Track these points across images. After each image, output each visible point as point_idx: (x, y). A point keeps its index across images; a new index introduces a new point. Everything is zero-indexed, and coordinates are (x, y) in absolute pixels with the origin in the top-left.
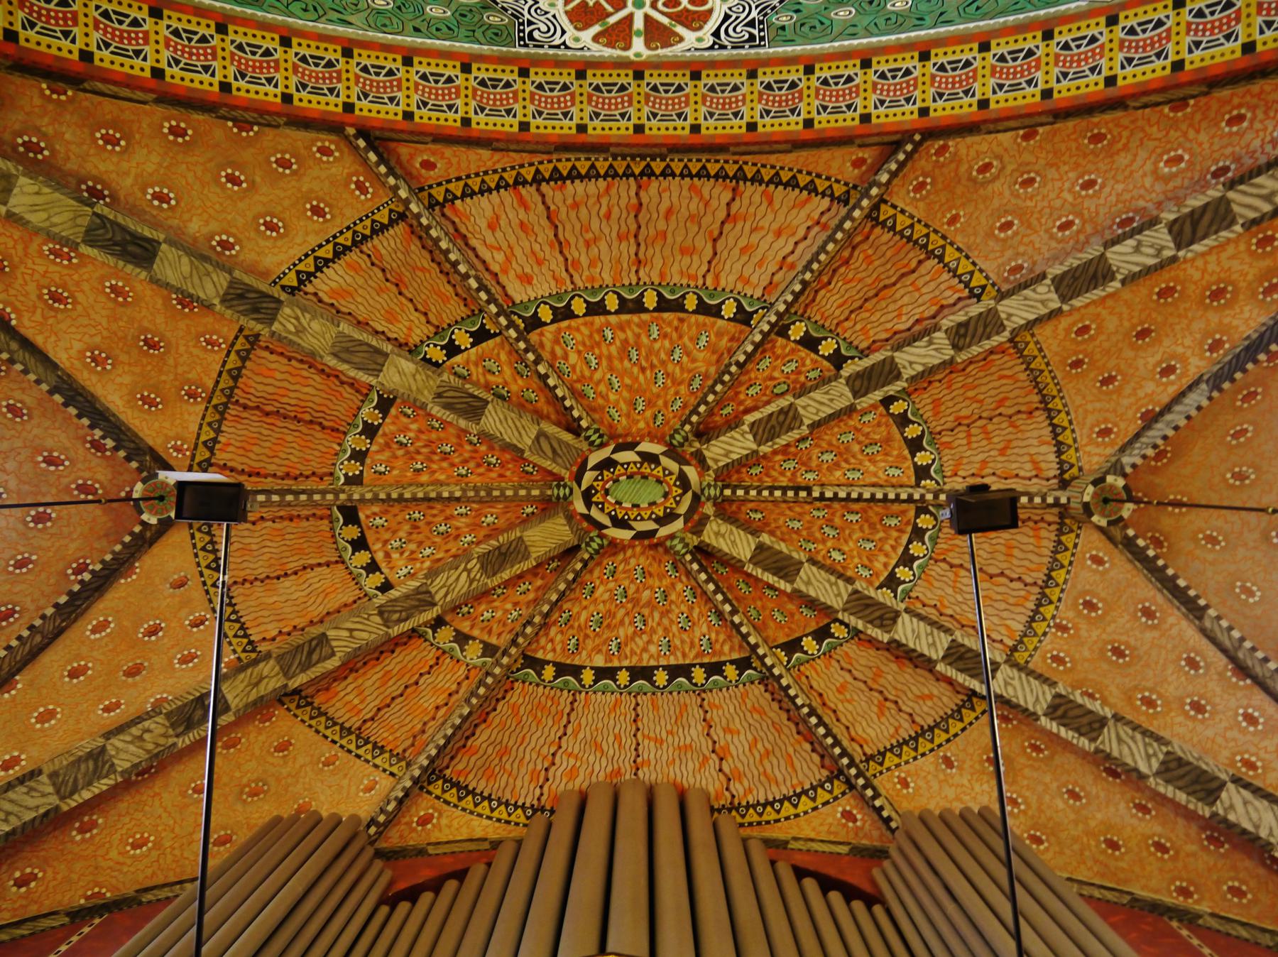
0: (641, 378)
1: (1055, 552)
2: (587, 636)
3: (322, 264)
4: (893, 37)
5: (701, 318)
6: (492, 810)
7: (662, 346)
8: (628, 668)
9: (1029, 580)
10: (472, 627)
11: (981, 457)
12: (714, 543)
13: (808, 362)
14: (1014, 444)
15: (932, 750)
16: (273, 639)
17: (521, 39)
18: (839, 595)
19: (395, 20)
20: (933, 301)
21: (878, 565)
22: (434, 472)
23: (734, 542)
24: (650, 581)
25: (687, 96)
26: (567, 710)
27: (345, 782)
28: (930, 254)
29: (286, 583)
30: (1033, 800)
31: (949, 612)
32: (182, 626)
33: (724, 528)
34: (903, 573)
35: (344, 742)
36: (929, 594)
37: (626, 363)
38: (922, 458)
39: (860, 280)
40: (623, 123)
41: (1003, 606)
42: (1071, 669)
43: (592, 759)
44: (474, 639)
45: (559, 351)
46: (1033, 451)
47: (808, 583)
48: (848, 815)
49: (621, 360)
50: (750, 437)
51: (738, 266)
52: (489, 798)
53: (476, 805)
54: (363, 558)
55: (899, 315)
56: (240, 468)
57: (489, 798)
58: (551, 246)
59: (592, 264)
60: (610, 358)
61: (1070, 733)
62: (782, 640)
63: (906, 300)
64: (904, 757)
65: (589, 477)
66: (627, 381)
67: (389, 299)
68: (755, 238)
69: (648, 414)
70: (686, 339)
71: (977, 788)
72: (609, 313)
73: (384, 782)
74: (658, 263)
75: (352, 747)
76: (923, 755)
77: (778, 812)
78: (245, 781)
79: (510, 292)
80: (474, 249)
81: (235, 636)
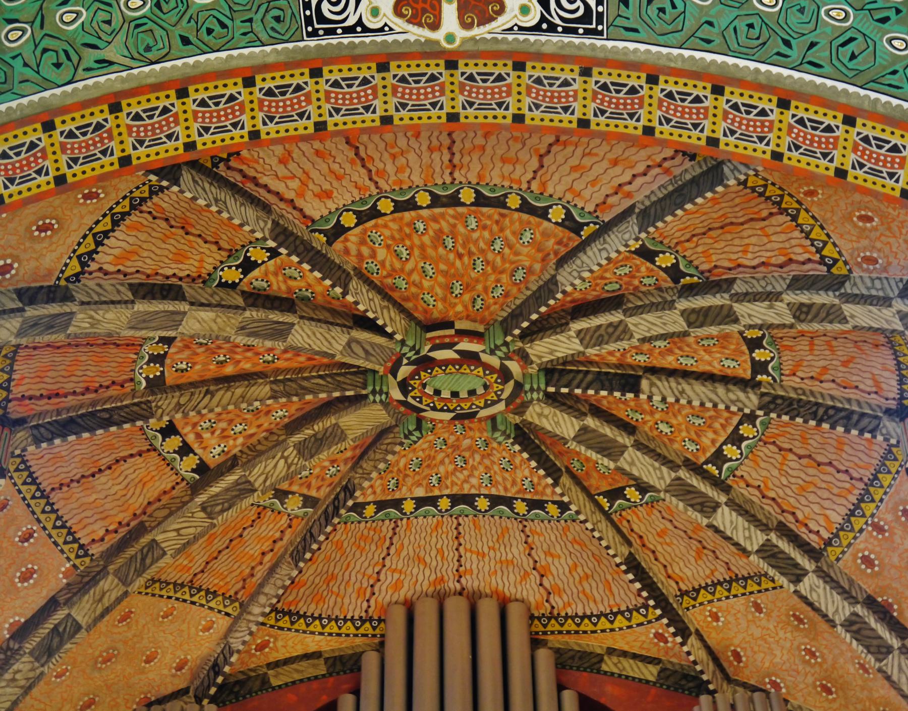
0: (458, 263)
1: (885, 458)
2: (406, 476)
3: (100, 239)
4: (752, 65)
5: (525, 216)
6: (323, 627)
7: (481, 236)
8: (448, 496)
9: (855, 475)
10: (291, 484)
11: (822, 363)
12: (537, 422)
13: (643, 269)
14: (857, 360)
15: (743, 594)
16: (102, 539)
17: (309, 21)
18: (663, 478)
19: (159, 32)
20: (782, 251)
21: (706, 441)
22: (239, 362)
23: (557, 423)
24: (471, 433)
25: (509, 86)
26: (390, 534)
28: (783, 211)
29: (102, 479)
30: (830, 658)
31: (772, 494)
32: (13, 544)
33: (547, 410)
34: (730, 451)
35: (178, 595)
36: (754, 475)
37: (441, 250)
38: (760, 355)
39: (705, 214)
40: (434, 113)
41: (826, 494)
43: (415, 571)
44: (293, 493)
45: (365, 251)
46: (876, 372)
47: (632, 464)
48: (660, 637)
49: (435, 248)
50: (577, 341)
51: (569, 179)
52: (320, 618)
53: (308, 625)
54: (174, 442)
55: (745, 252)
56: (38, 394)
57: (320, 618)
58: (352, 162)
59: (399, 170)
60: (423, 247)
61: (861, 648)
62: (605, 488)
63: (753, 240)
64: (717, 595)
65: (404, 371)
66: (442, 267)
67: (179, 241)
68: (587, 162)
69: (467, 297)
70: (508, 233)
71: (781, 634)
72: (421, 208)
73: (221, 621)
74: (476, 167)
75: (187, 597)
76: (735, 596)
77: (595, 625)
78: (97, 653)
79: (308, 212)
80: (265, 187)
81: (65, 543)
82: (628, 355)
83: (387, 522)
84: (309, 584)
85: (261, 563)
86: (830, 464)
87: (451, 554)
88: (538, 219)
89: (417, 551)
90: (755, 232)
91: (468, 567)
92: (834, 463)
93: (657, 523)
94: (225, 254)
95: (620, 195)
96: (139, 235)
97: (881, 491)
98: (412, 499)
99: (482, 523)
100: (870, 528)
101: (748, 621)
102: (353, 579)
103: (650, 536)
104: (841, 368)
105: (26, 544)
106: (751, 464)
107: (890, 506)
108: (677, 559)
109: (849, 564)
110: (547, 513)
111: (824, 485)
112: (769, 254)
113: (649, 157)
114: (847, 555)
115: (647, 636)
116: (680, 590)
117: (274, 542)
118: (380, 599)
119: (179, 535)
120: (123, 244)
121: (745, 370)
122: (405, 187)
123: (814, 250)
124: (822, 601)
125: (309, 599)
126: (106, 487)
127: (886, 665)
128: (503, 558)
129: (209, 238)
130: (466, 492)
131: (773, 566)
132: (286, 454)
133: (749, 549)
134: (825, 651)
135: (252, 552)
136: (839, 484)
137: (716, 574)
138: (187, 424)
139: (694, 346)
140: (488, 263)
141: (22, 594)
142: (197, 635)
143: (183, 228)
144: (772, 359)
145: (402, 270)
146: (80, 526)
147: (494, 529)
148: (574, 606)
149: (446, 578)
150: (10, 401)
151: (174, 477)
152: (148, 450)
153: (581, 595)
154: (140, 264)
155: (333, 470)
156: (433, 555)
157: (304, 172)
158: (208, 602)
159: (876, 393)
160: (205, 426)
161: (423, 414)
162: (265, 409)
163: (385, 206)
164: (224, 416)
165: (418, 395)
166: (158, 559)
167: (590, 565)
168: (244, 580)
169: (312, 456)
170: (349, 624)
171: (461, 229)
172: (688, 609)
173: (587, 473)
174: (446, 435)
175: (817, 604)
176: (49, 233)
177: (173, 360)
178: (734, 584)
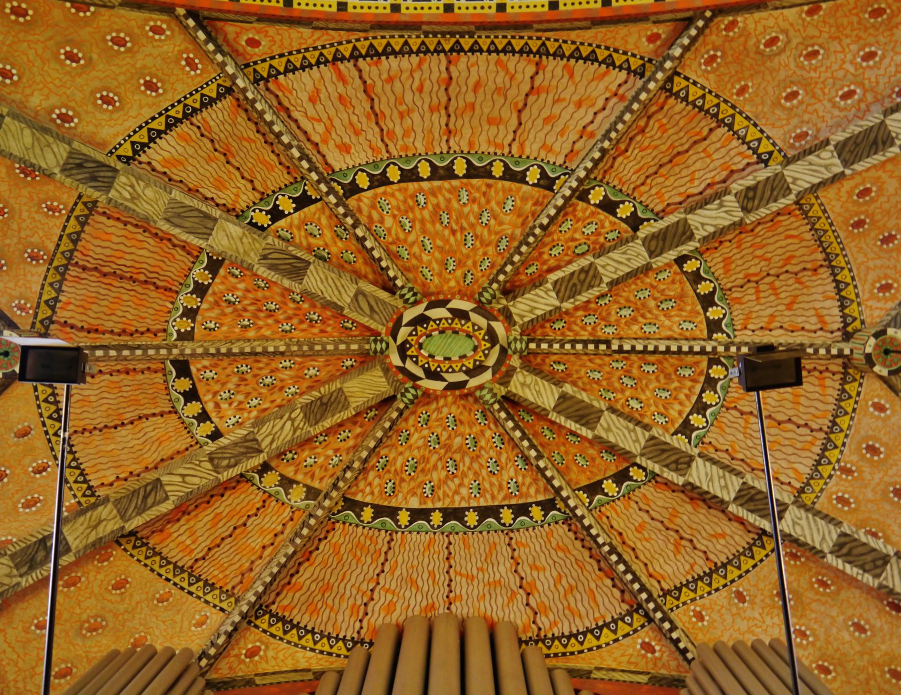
0: (452, 239)
1: (840, 400)
3: (155, 136)
5: (507, 184)
6: (315, 643)
7: (471, 211)
8: (440, 510)
9: (815, 426)
11: (769, 311)
12: (520, 393)
13: (607, 224)
15: (725, 586)
20: (724, 166)
21: (673, 413)
22: (261, 328)
23: (538, 392)
26: (385, 549)
27: (178, 618)
28: (721, 123)
29: (123, 432)
31: (740, 456)
32: (26, 472)
34: (696, 420)
35: (177, 580)
36: (721, 440)
37: (438, 226)
38: (714, 313)
39: (656, 147)
41: (790, 450)
42: (856, 510)
43: (408, 594)
44: (298, 483)
45: (375, 216)
49: (433, 223)
50: (553, 294)
51: (541, 135)
53: (300, 638)
54: (194, 408)
55: (692, 180)
56: (80, 325)
57: (313, 632)
58: (368, 117)
59: (406, 134)
60: (423, 222)
61: (855, 570)
62: (584, 483)
63: (698, 165)
64: (699, 592)
65: (404, 333)
66: (439, 243)
68: (557, 110)
69: (459, 273)
70: (493, 204)
71: (768, 621)
72: (422, 179)
73: (214, 617)
75: (185, 584)
76: (717, 590)
77: (582, 643)
78: (84, 617)
79: (330, 161)
80: (296, 121)
81: (76, 482)
82: (598, 328)
83: (383, 532)
84: (305, 589)
85: (261, 557)
86: (790, 421)
87: (442, 578)
88: (518, 185)
89: (410, 571)
90: (698, 156)
91: (458, 593)
92: (794, 419)
93: (635, 516)
94: (258, 196)
95: (585, 138)
96: (187, 147)
97: (842, 435)
98: (407, 510)
99: (471, 541)
100: (838, 473)
101: (733, 615)
102: (348, 592)
103: (629, 532)
104: (786, 313)
105: (38, 476)
106: (717, 430)
107: (853, 447)
108: (657, 556)
109: (826, 505)
110: (532, 518)
111: (787, 442)
112: (713, 174)
113: (607, 88)
114: (821, 499)
115: (634, 647)
116: (662, 589)
117: (276, 535)
118: (373, 621)
119: (184, 482)
120: (173, 151)
121: (701, 331)
122: (410, 154)
123: (751, 152)
124: (807, 533)
125: (304, 607)
126: (126, 440)
127: (886, 578)
128: (491, 580)
129: (246, 175)
130: (456, 505)
131: (752, 511)
132: (293, 416)
133: (726, 498)
134: (815, 627)
135: (253, 545)
136: (801, 439)
137: (696, 568)
138: (208, 391)
139: (655, 312)
140: (477, 237)
141: (21, 518)
142: (189, 629)
143: (225, 155)
144: (725, 315)
145: (405, 241)
146: (94, 470)
147: (482, 547)
148: (560, 625)
149: (437, 605)
150: (53, 322)
151: (189, 440)
152: (170, 412)
153: (566, 612)
154: (184, 175)
155: (336, 459)
156: (425, 578)
157: (329, 118)
158: (205, 594)
159: (821, 329)
160: (225, 396)
161: (418, 383)
162: (279, 384)
163: (394, 174)
164: (242, 388)
165: (415, 353)
166: (160, 502)
167: (574, 574)
168: (243, 575)
169: (316, 423)
170: (341, 643)
171: (455, 204)
172: (672, 610)
173: (567, 467)
174: (439, 430)
175: (802, 538)
176: (110, 107)
177: (204, 318)
178: (714, 576)
